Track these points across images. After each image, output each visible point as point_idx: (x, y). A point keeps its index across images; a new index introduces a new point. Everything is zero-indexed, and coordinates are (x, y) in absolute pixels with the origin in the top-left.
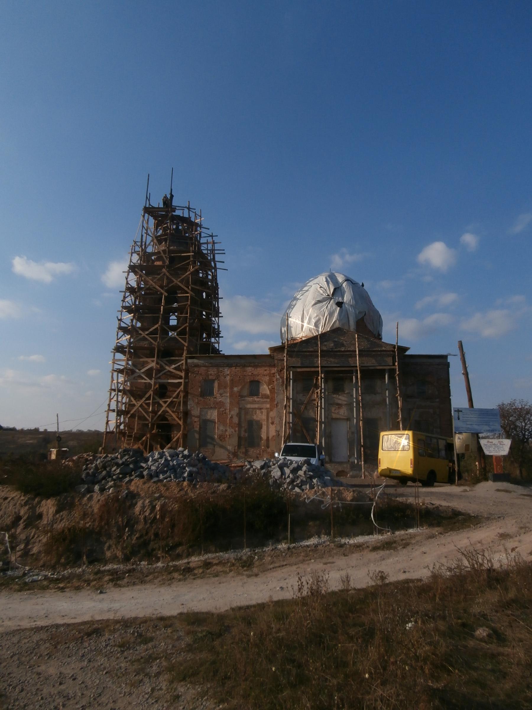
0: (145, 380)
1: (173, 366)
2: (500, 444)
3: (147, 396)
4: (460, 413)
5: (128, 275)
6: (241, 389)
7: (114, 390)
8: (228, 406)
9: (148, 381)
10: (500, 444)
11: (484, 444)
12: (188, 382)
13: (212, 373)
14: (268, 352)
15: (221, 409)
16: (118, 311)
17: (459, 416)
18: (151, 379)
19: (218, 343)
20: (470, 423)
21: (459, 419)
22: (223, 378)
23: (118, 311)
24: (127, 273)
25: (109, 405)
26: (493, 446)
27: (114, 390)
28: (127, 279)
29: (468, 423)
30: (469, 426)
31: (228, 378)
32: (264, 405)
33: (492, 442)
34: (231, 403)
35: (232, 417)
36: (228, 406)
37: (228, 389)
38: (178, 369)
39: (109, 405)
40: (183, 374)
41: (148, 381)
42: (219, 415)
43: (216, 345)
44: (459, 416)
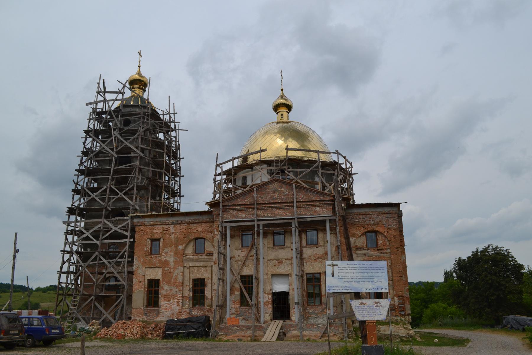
0: (93, 241)
1: (120, 226)
2: (376, 306)
3: (93, 257)
4: (335, 267)
5: (86, 140)
6: (186, 247)
7: (68, 252)
8: (172, 264)
9: (96, 242)
10: (376, 306)
11: (357, 307)
12: (134, 241)
13: (158, 231)
14: (206, 208)
15: (166, 269)
16: (75, 175)
17: (333, 272)
18: (97, 239)
19: (179, 203)
20: (349, 280)
21: (333, 275)
22: (168, 236)
23: (75, 175)
24: (84, 139)
25: (61, 268)
26: (368, 309)
27: (68, 252)
28: (84, 144)
29: (345, 280)
30: (347, 284)
31: (173, 236)
32: (209, 262)
33: (365, 304)
34: (176, 262)
35: (176, 277)
36: (172, 264)
37: (173, 248)
38: (124, 229)
39: (61, 268)
40: (128, 234)
41: (96, 242)
42: (164, 274)
43: (176, 206)
44: (333, 272)
